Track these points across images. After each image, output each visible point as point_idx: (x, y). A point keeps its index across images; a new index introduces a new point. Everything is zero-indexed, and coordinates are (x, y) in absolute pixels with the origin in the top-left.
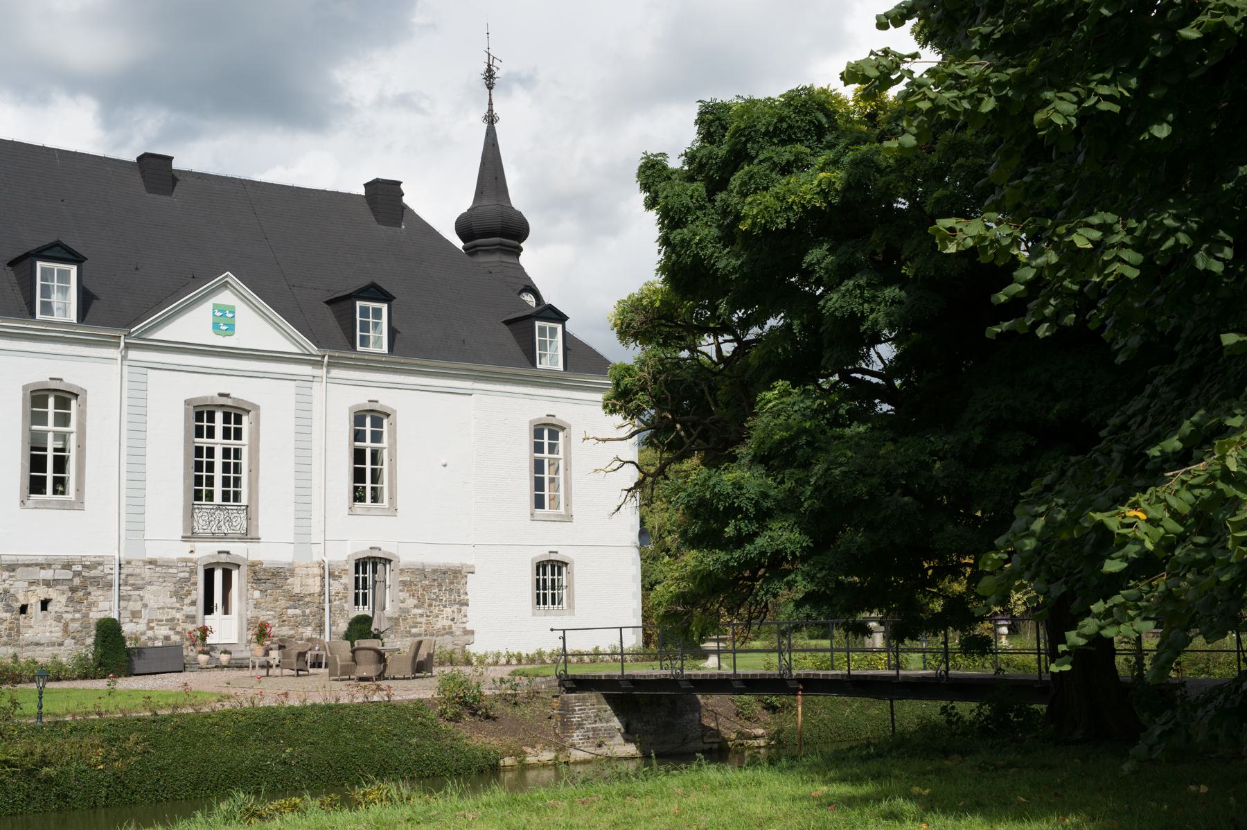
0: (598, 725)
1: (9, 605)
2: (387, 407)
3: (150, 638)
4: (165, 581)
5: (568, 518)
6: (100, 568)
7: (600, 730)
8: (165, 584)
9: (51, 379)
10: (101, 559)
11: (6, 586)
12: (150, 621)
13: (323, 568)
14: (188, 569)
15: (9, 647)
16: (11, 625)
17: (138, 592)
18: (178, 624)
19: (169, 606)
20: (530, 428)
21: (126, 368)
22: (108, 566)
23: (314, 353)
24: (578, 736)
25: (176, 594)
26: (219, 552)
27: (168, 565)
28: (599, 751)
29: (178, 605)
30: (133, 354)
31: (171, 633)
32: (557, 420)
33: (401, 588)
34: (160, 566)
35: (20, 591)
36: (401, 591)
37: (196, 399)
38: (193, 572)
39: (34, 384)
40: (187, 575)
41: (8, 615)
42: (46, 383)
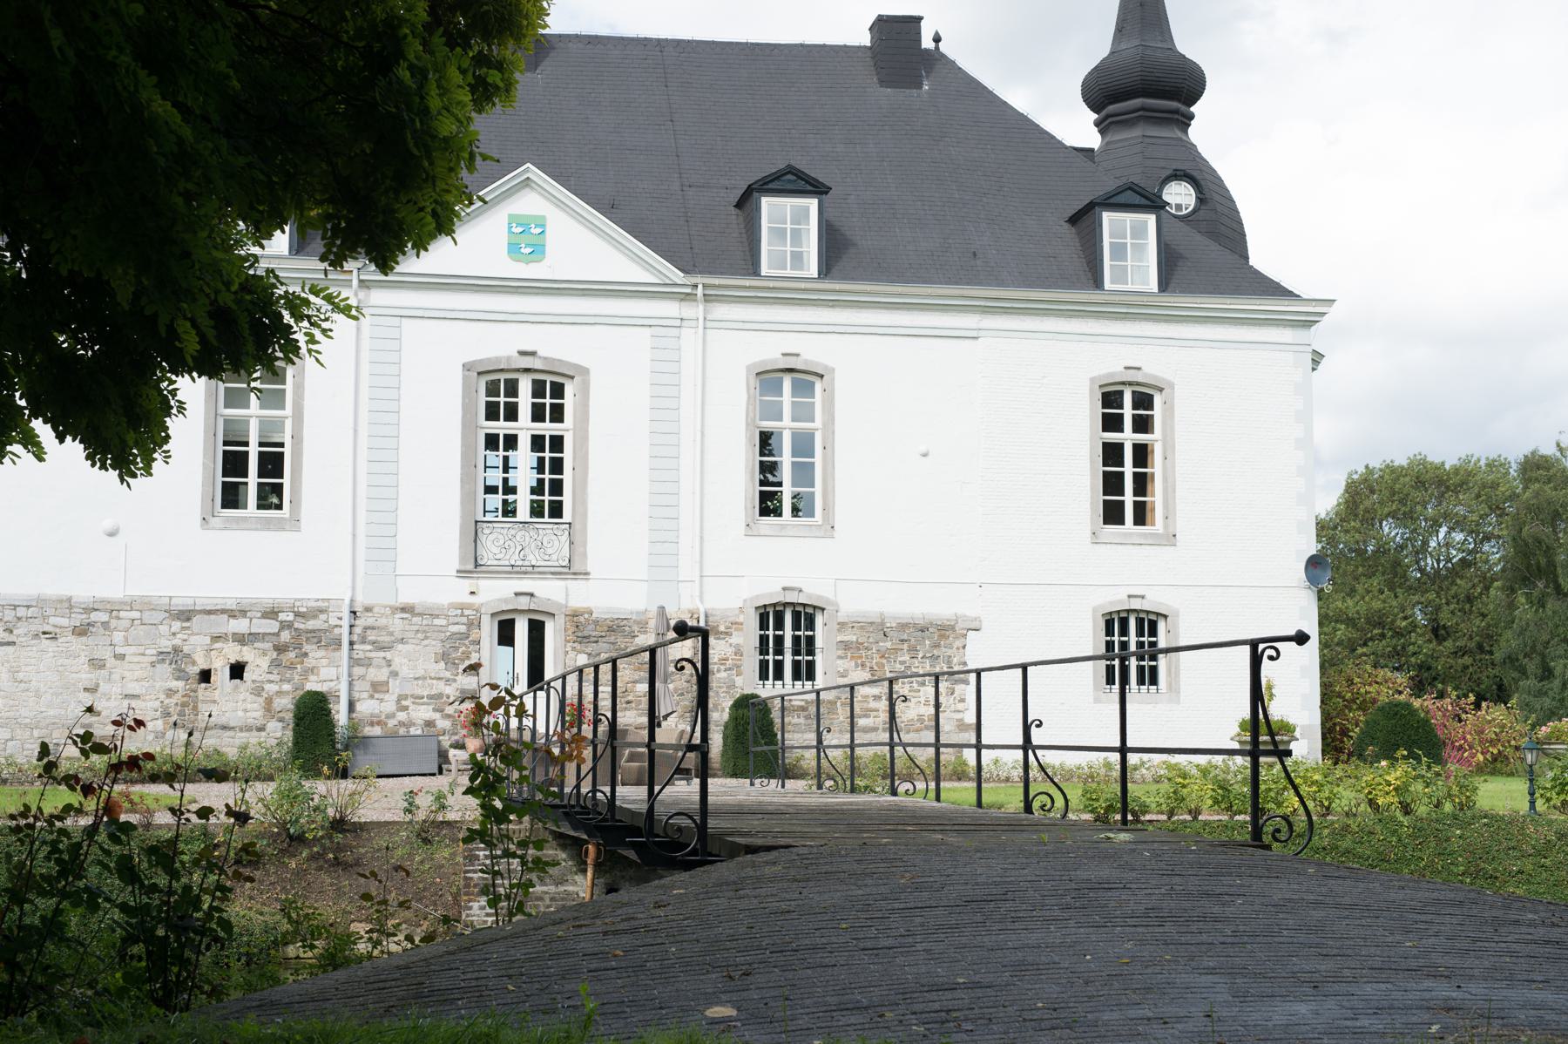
3: (402, 724)
4: (426, 638)
5: (1171, 538)
6: (323, 617)
8: (426, 642)
11: (177, 641)
12: (401, 698)
14: (464, 620)
16: (185, 699)
17: (382, 654)
19: (433, 675)
20: (1091, 391)
22: (335, 614)
29: (448, 675)
33: (840, 653)
35: (199, 649)
36: (840, 657)
38: (474, 624)
40: (463, 629)
41: (180, 684)
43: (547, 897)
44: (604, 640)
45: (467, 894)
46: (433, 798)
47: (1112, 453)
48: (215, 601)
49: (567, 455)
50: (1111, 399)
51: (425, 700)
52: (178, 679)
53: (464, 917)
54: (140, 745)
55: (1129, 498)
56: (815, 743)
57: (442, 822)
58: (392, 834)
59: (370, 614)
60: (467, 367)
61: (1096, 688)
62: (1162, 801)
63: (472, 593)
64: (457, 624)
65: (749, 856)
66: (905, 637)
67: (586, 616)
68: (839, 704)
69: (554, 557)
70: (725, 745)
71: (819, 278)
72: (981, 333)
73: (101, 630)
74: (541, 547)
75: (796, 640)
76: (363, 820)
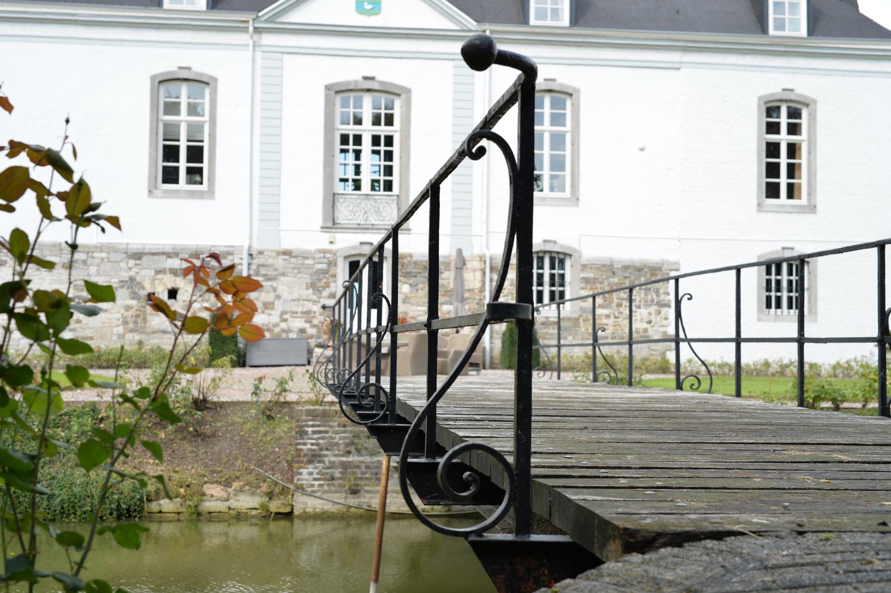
0: (353, 458)
1: (134, 293)
2: (568, 86)
3: (283, 331)
4: (300, 272)
5: (812, 208)
6: (230, 258)
7: (358, 467)
8: (300, 275)
9: (180, 68)
10: (232, 249)
11: (132, 273)
12: (283, 313)
13: (485, 262)
14: (326, 261)
15: (135, 334)
16: (138, 313)
17: (270, 283)
18: (314, 317)
19: (304, 298)
20: (759, 105)
21: (259, 55)
22: (238, 256)
23: (473, 28)
24: (311, 474)
25: (313, 286)
26: (362, 243)
27: (304, 255)
28: (353, 501)
29: (315, 298)
30: (268, 39)
31: (307, 326)
32: (797, 95)
33: (582, 285)
34: (296, 257)
35: (147, 279)
36: (582, 288)
37: (337, 84)
38: (332, 263)
39: (162, 74)
40: (324, 266)
41: (134, 303)
42: (174, 72)
43: (363, 466)
44: (421, 275)
45: (298, 462)
46: (277, 384)
47: (772, 149)
48: (158, 247)
49: (396, 149)
50: (771, 111)
51: (299, 315)
52: (133, 299)
53: (295, 481)
54: (107, 343)
55: (783, 180)
56: (591, 342)
57: (285, 403)
58: (244, 411)
59: (262, 256)
60: (328, 88)
61: (760, 311)
62: (858, 392)
63: (331, 242)
64: (321, 263)
65: (636, 558)
66: (627, 275)
67: (409, 259)
68: (581, 320)
69: (387, 218)
70: (503, 347)
71: (570, 26)
72: (683, 65)
73: (82, 266)
74: (378, 212)
75: (552, 276)
76: (223, 399)
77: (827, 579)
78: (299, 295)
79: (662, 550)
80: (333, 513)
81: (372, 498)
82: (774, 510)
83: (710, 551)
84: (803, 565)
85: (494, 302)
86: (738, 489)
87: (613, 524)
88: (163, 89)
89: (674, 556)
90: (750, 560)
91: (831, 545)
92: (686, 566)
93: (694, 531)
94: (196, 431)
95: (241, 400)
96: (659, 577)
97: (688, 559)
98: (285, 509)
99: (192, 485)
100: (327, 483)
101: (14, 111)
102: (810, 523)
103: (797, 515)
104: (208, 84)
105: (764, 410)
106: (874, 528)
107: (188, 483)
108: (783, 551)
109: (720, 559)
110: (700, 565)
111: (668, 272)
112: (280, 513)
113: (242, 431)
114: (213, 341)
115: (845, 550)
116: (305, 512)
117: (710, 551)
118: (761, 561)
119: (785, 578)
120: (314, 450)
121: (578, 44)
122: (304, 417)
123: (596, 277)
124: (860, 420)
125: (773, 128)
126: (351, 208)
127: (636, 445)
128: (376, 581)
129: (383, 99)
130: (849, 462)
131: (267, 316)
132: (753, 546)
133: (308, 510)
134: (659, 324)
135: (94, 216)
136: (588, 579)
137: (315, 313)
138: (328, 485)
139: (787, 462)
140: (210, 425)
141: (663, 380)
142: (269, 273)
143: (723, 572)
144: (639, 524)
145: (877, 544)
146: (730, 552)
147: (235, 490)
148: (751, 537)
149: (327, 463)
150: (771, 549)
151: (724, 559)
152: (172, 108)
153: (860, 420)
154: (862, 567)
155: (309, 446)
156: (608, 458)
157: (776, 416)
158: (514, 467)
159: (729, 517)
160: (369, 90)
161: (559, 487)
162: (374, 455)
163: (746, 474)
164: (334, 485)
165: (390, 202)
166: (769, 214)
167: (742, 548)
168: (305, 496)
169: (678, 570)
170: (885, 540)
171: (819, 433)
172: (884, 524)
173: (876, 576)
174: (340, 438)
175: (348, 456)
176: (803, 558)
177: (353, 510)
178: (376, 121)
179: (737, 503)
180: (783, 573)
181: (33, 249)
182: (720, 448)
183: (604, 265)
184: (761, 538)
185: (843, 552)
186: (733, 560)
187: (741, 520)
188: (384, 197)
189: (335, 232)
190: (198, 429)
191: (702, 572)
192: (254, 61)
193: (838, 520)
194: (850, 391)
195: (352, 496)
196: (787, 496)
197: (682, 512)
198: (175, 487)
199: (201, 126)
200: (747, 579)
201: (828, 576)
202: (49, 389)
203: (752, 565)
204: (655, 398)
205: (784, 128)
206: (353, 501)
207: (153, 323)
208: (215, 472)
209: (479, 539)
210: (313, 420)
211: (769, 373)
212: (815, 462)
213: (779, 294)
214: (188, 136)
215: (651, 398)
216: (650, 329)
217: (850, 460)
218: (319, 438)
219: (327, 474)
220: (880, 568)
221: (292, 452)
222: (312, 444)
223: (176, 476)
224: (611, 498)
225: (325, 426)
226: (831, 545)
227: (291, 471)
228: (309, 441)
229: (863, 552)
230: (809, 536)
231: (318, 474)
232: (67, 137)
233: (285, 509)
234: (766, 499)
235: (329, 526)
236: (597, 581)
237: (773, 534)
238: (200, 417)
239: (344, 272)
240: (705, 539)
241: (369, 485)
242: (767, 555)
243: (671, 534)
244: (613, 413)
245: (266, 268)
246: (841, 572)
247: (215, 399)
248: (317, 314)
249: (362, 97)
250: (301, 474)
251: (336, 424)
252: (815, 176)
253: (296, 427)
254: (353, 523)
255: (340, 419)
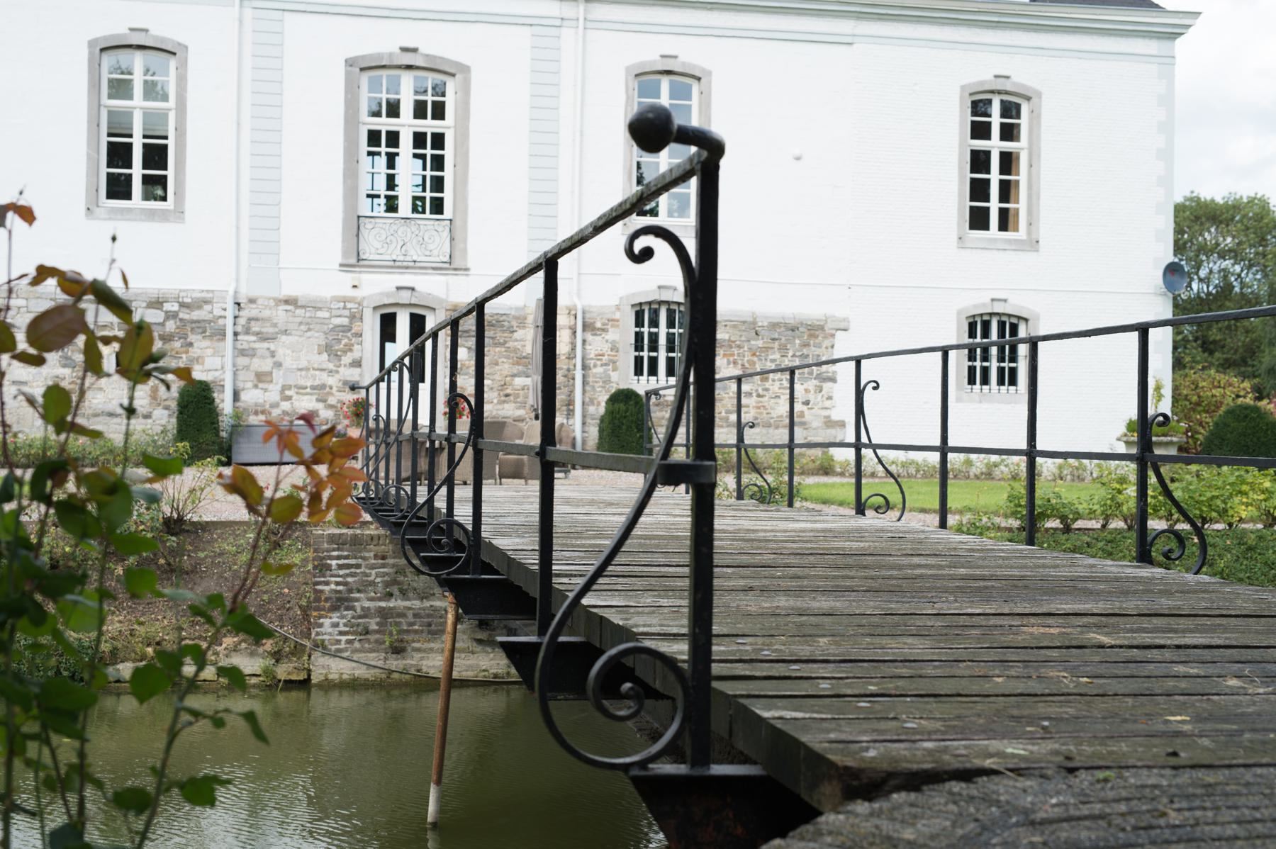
0: (397, 603)
4: (309, 330)
5: (1033, 244)
6: (207, 307)
7: (403, 615)
8: (309, 334)
9: (132, 30)
10: (210, 295)
12: (285, 388)
14: (347, 313)
17: (265, 345)
18: (330, 394)
19: (316, 366)
20: (962, 98)
21: (248, 13)
22: (219, 305)
24: (336, 625)
25: (328, 348)
28: (395, 663)
29: (331, 366)
31: (320, 406)
32: (1014, 84)
34: (303, 307)
37: (363, 57)
38: (356, 317)
39: (105, 38)
40: (345, 321)
47: (979, 161)
49: (448, 153)
50: (980, 107)
51: (308, 390)
52: (64, 366)
53: (313, 636)
55: (994, 205)
60: (350, 63)
62: (1096, 507)
63: (355, 286)
64: (340, 316)
65: (862, 807)
70: (601, 437)
72: (856, 39)
76: (206, 518)
77: (1111, 839)
78: (309, 362)
79: (895, 796)
80: (366, 680)
81: (422, 659)
82: (1030, 732)
83: (957, 798)
84: (1079, 819)
85: (663, 462)
86: (976, 696)
87: (828, 760)
88: (108, 60)
89: (912, 805)
90: (1011, 812)
91: (1112, 788)
92: (928, 819)
93: (933, 768)
94: (169, 564)
95: (232, 519)
96: (896, 835)
97: (930, 809)
98: (298, 675)
99: (165, 643)
100: (358, 638)
101: (36, 224)
102: (1080, 753)
103: (1062, 740)
104: (174, 54)
105: (982, 550)
106: (1162, 760)
107: (158, 639)
108: (1051, 797)
109: (972, 810)
110: (947, 819)
111: (834, 332)
112: (291, 681)
113: (235, 564)
114: (183, 428)
115: (1130, 796)
116: (327, 679)
117: (957, 798)
118: (1026, 812)
119: (1058, 838)
120: (339, 592)
121: (709, 6)
122: (326, 545)
123: (732, 339)
124: (1113, 569)
125: (980, 131)
126: (384, 237)
127: (829, 619)
128: (438, 782)
129: (430, 79)
130: (1112, 647)
131: (262, 391)
132: (1013, 791)
133: (331, 677)
134: (820, 405)
135: (156, 369)
136: (802, 839)
137: (331, 388)
138: (360, 640)
139: (1032, 648)
140: (189, 556)
141: (825, 485)
142: (265, 330)
143: (978, 830)
144: (862, 759)
145: (1170, 786)
146: (983, 799)
147: (226, 649)
148: (1008, 777)
149: (359, 610)
150: (1035, 795)
151: (978, 810)
152: (120, 88)
153: (1113, 569)
154: (1154, 822)
155: (333, 586)
156: (794, 642)
157: (1000, 562)
158: (688, 675)
159: (974, 745)
160: (409, 67)
161: (742, 696)
162: (426, 598)
163: (979, 670)
164: (368, 641)
165: (440, 229)
166: (974, 251)
167: (999, 795)
168: (327, 657)
169: (919, 826)
170: (1179, 780)
171: (1063, 593)
172: (1175, 754)
173: (1173, 834)
174: (377, 575)
175: (388, 600)
176: (1079, 809)
177: (396, 676)
178: (420, 111)
179: (981, 721)
180: (1055, 830)
181: (75, 415)
182: (939, 623)
183: (744, 322)
184: (1021, 779)
185: (1128, 799)
186: (988, 812)
187: (991, 750)
188: (432, 222)
189: (360, 272)
190: (171, 561)
191: (950, 829)
192: (241, 22)
193: (1115, 749)
194: (1085, 505)
195: (394, 656)
196: (1042, 709)
197: (913, 738)
198: (140, 645)
199: (163, 116)
200: (1010, 840)
201: (1112, 835)
202: (101, 602)
203: (1014, 820)
204: (830, 531)
205: (996, 131)
206: (395, 663)
207: (95, 401)
208: (197, 624)
209: (643, 773)
210: (338, 549)
211: (972, 474)
212: (1068, 647)
213: (985, 364)
214: (144, 129)
215: (824, 530)
216: (806, 412)
217: (1113, 643)
218: (347, 575)
219: (358, 625)
220: (1177, 822)
221: (308, 595)
222: (337, 584)
223: (141, 630)
224: (815, 715)
225: (356, 558)
226: (1112, 788)
227: (306, 623)
228: (333, 579)
229: (1153, 799)
230: (1082, 774)
231: (345, 625)
232: (113, 261)
233: (298, 675)
234: (1015, 712)
235: (361, 698)
236: (815, 841)
237: (1037, 772)
238: (175, 545)
239: (373, 329)
240: (950, 779)
241: (419, 641)
242: (1032, 803)
243: (907, 774)
244: (780, 560)
245: (258, 323)
246: (1129, 828)
247: (195, 519)
248: (335, 389)
249: (399, 77)
250: (321, 625)
251: (372, 554)
252: (1038, 198)
253: (314, 559)
254: (396, 692)
255: (377, 548)
